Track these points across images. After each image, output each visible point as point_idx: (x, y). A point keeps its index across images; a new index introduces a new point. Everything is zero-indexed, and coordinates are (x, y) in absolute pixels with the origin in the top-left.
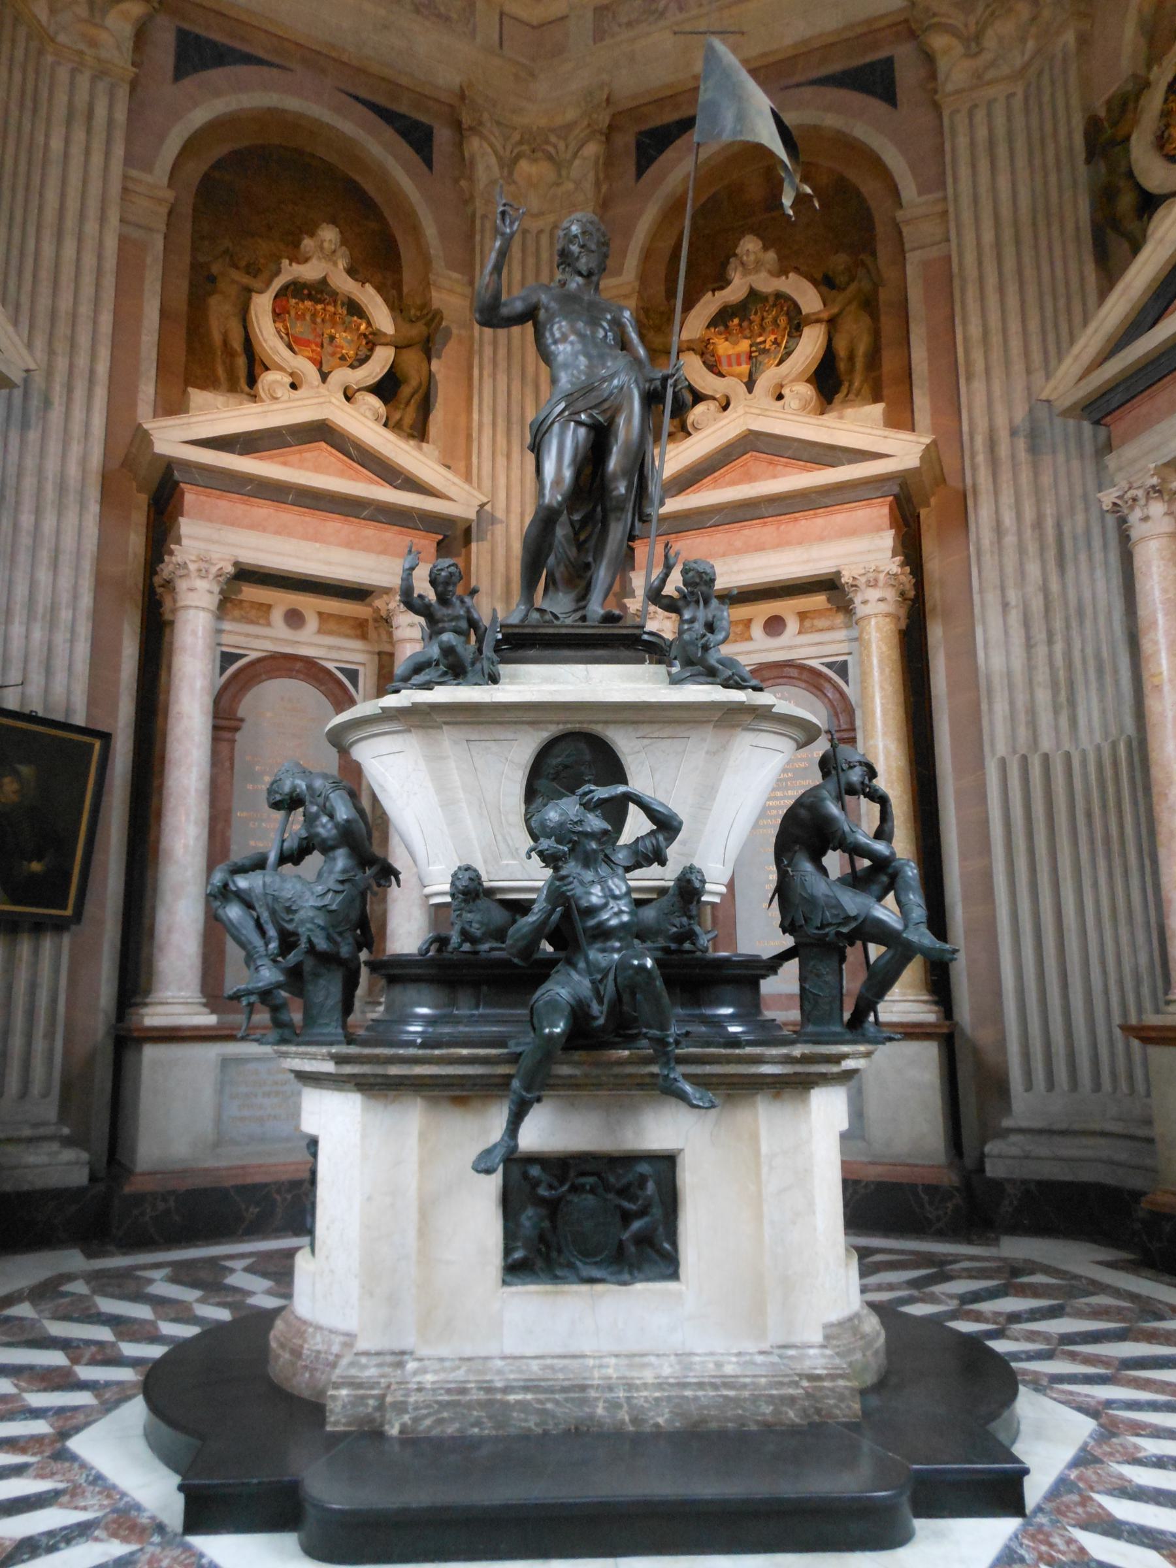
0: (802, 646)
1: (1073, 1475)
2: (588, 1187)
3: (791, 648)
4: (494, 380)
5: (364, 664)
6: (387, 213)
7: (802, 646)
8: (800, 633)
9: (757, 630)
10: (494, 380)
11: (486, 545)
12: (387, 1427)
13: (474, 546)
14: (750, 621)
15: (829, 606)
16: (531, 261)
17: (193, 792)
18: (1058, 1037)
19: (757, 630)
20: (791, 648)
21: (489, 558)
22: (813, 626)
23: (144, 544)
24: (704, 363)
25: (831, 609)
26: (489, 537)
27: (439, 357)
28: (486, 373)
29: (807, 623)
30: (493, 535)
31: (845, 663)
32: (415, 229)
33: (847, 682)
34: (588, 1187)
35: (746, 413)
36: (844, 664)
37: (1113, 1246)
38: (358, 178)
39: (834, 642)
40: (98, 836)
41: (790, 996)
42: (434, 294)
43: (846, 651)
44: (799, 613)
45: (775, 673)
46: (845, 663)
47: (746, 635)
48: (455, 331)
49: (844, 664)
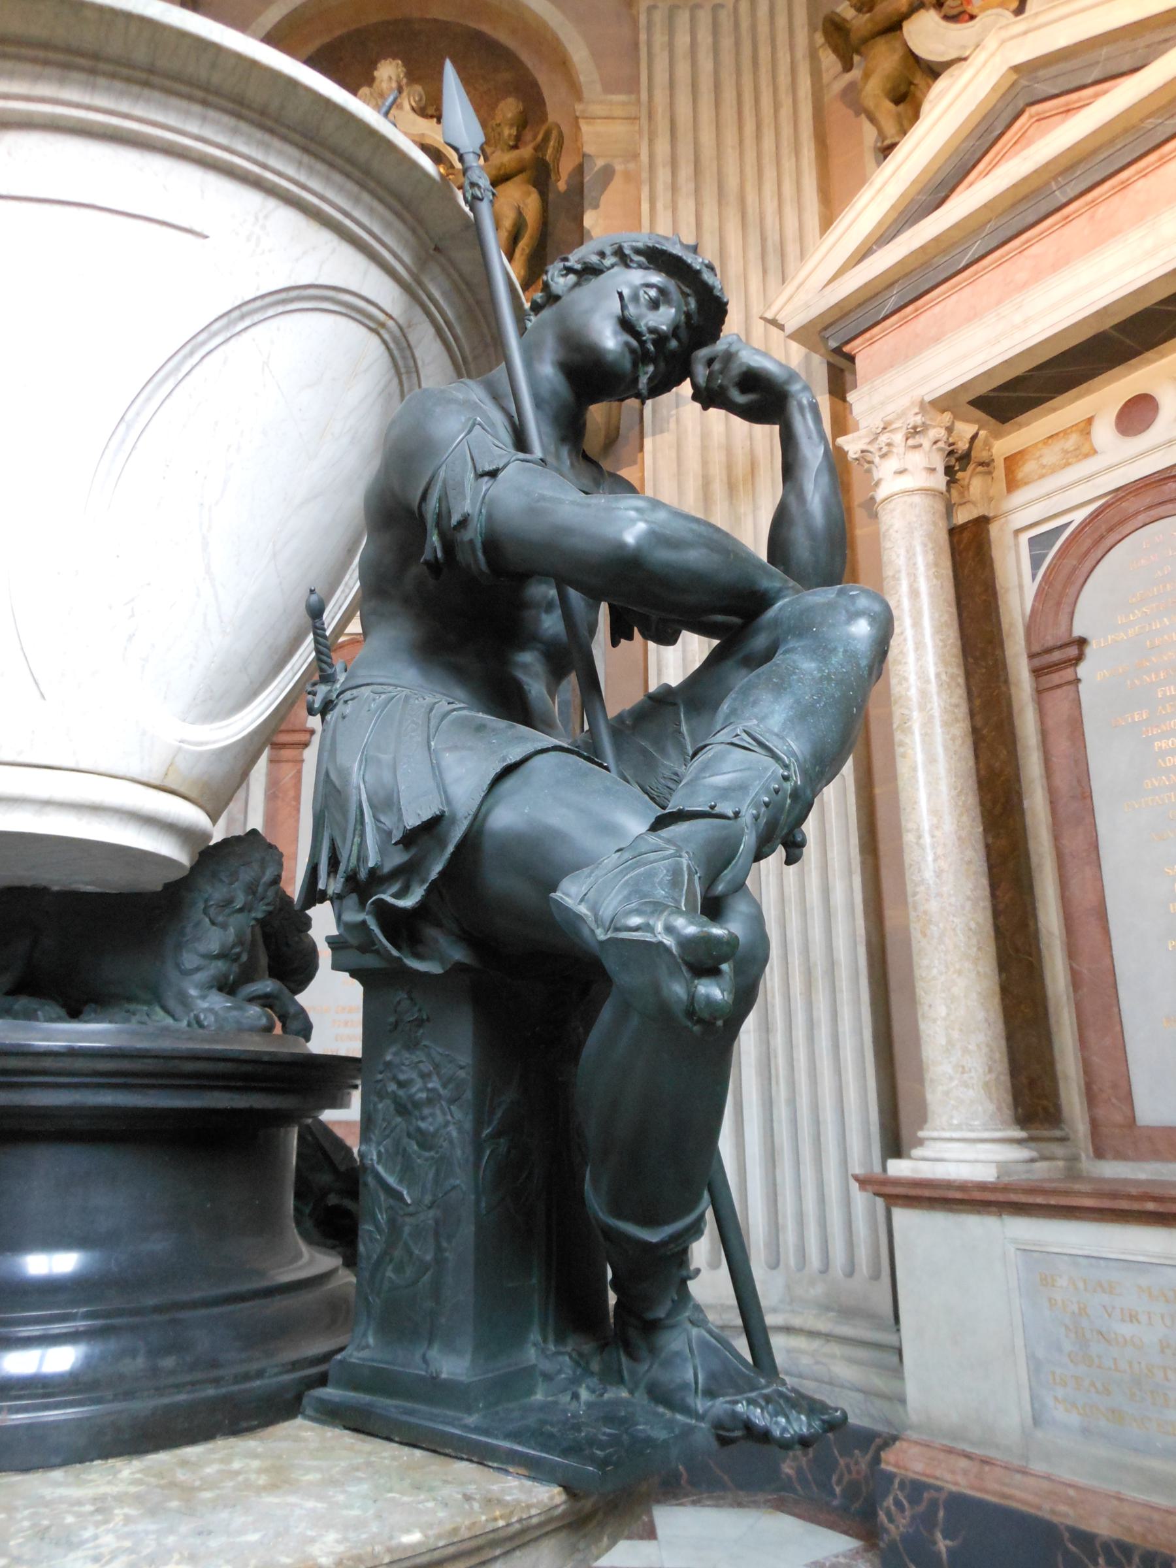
4: (674, 210)
6: (526, 57)
9: (1104, 432)
10: (674, 210)
11: (668, 438)
13: (648, 443)
14: (1090, 421)
16: (727, 43)
17: (1064, 998)
18: (747, 79)
19: (1104, 432)
21: (674, 455)
24: (947, 18)
26: (673, 425)
27: (596, 207)
28: (660, 205)
30: (678, 421)
32: (562, 64)
35: (1003, 42)
38: (485, 28)
40: (897, 1028)
41: (354, 1123)
42: (585, 127)
45: (1148, 498)
48: (619, 167)
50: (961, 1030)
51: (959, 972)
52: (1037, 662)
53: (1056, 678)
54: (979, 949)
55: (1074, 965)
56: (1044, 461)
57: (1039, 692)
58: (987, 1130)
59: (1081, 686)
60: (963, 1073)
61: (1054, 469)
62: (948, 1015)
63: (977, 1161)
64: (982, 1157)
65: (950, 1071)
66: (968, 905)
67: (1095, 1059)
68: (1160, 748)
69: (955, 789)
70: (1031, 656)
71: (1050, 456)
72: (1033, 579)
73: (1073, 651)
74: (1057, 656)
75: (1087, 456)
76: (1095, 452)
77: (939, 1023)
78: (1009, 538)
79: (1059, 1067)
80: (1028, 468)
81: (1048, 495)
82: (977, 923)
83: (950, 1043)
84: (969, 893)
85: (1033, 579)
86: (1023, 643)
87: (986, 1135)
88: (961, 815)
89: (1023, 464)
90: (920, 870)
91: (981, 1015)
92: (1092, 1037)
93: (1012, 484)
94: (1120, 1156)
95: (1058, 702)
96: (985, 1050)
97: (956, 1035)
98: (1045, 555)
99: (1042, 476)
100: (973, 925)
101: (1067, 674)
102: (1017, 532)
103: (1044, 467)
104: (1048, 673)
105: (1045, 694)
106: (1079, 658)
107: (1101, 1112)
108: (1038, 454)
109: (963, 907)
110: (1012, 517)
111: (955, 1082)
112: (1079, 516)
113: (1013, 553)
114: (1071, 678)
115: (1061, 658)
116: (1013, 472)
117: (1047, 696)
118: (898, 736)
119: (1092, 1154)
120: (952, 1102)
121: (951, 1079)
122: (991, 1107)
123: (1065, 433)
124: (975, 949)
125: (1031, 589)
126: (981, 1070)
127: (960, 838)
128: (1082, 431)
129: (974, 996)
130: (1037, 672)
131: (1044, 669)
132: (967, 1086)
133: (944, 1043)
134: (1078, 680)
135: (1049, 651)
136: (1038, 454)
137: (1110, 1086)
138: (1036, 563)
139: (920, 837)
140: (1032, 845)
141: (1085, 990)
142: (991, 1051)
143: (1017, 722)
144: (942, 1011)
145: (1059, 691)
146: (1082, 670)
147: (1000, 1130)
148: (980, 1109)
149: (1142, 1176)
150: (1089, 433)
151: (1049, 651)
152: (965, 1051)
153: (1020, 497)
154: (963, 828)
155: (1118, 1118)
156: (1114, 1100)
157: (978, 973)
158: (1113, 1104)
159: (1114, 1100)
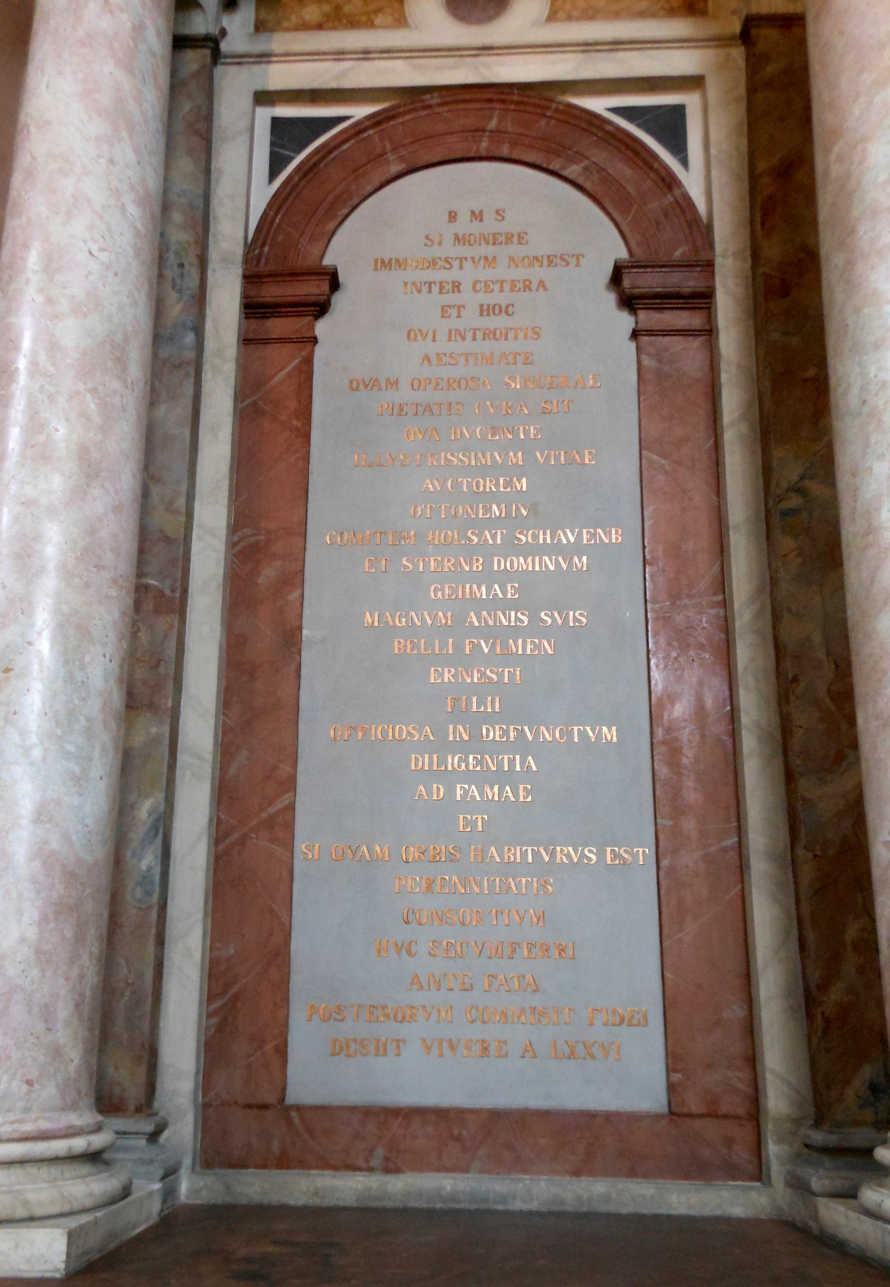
5: (694, 82)
31: (679, 111)
33: (685, 163)
46: (679, 111)
53: (277, 326)
98: (290, 159)
102: (263, 98)
106: (321, 308)
112: (360, 112)
125: (262, 194)
146: (322, 328)
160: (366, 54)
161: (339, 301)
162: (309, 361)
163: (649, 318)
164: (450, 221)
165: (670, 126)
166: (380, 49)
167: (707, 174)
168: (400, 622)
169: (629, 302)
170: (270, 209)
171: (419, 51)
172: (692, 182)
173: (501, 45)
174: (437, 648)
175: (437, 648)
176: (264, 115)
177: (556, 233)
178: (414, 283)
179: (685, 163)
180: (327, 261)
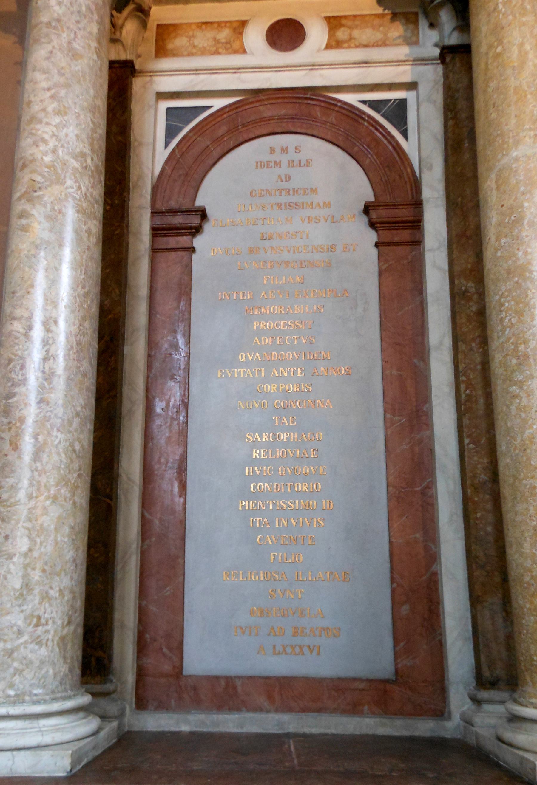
0: (332, 65)
1: (483, 302)
2: (308, 631)
3: (313, 66)
5: (412, 86)
7: (332, 65)
8: (328, 47)
12: (98, 137)
14: (243, 24)
15: (380, 10)
17: (134, 546)
19: (255, 37)
20: (313, 66)
22: (351, 38)
23: (82, 639)
25: (382, 16)
29: (341, 34)
31: (402, 104)
33: (405, 134)
34: (308, 631)
36: (401, 105)
37: (437, 589)
39: (388, 62)
43: (407, 79)
44: (329, 19)
46: (402, 104)
47: (236, 45)
49: (401, 105)
50: (44, 571)
51: (55, 499)
52: (159, 222)
53: (172, 242)
54: (80, 476)
55: (146, 514)
56: (196, 42)
57: (154, 250)
58: (55, 699)
59: (194, 256)
60: (37, 625)
61: (203, 52)
62: (30, 550)
63: (39, 747)
64: (47, 739)
65: (20, 623)
66: (76, 421)
67: (153, 608)
68: (258, 327)
69: (83, 287)
70: (155, 213)
71: (203, 39)
72: (166, 147)
73: (195, 221)
74: (178, 220)
75: (236, 52)
76: (245, 52)
77: (15, 559)
78: (151, 98)
79: (117, 615)
80: (179, 42)
81: (196, 71)
82: (82, 446)
83: (27, 586)
84: (79, 409)
85: (166, 147)
86: (149, 197)
87: (56, 706)
88: (84, 319)
89: (175, 37)
90: (23, 367)
91: (69, 555)
92: (152, 584)
93: (161, 51)
94: (162, 706)
95: (170, 263)
96: (68, 596)
97: (36, 576)
98: (181, 129)
99: (190, 54)
100: (77, 447)
101: (183, 241)
102: (162, 96)
103: (195, 47)
104: (165, 235)
105: (159, 254)
106: (197, 230)
107: (149, 661)
108: (191, 33)
109: (70, 423)
110: (156, 79)
111: (26, 638)
112: (218, 103)
113: (152, 111)
114: (188, 245)
115: (180, 224)
116: (163, 40)
117: (160, 256)
118: (19, 207)
119: (134, 706)
120: (16, 664)
121: (20, 633)
122: (64, 669)
123: (219, 25)
124: (75, 475)
125: (162, 155)
126: (59, 622)
127: (79, 343)
128: (235, 30)
129: (66, 530)
130: (156, 232)
131: (163, 229)
132: (39, 643)
133: (18, 586)
134: (192, 250)
135: (173, 212)
136: (191, 33)
137: (162, 636)
138: (170, 133)
139: (30, 328)
140: (126, 390)
141: (154, 539)
142: (74, 598)
143: (131, 270)
144: (22, 544)
145: (173, 254)
146: (198, 242)
147: (69, 698)
148: (51, 672)
149: (185, 728)
150: (241, 34)
151: (173, 212)
152: (45, 597)
153: (165, 64)
154: (84, 335)
155: (167, 668)
156: (165, 650)
157: (74, 503)
158: (164, 655)
159: (165, 650)
160: (196, 71)
161: (207, 227)
162: (188, 268)
163: (388, 236)
164: (271, 153)
165: (398, 113)
166: (312, 64)
167: (423, 145)
168: (255, 578)
169: (372, 225)
170: (166, 165)
171: (328, 65)
172: (409, 146)
173: (200, 68)
174: (270, 455)
175: (270, 455)
176: (164, 105)
177: (332, 176)
178: (315, 636)
179: (405, 134)
180: (199, 203)
